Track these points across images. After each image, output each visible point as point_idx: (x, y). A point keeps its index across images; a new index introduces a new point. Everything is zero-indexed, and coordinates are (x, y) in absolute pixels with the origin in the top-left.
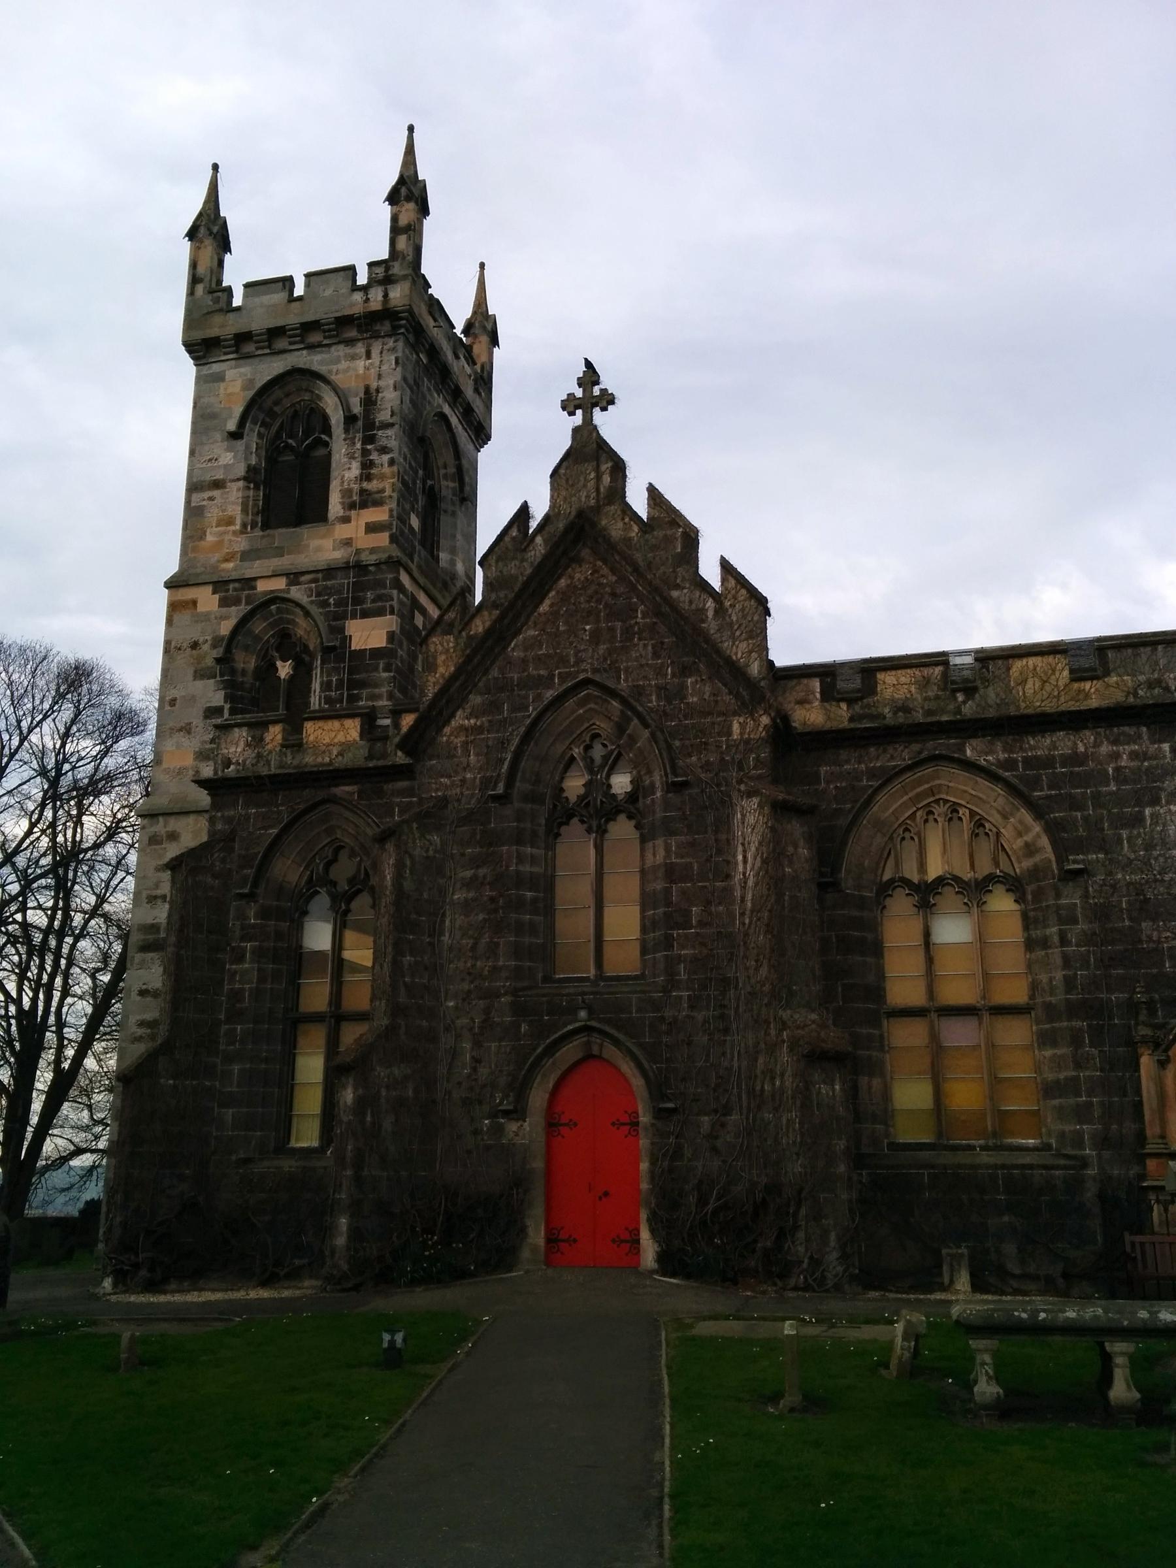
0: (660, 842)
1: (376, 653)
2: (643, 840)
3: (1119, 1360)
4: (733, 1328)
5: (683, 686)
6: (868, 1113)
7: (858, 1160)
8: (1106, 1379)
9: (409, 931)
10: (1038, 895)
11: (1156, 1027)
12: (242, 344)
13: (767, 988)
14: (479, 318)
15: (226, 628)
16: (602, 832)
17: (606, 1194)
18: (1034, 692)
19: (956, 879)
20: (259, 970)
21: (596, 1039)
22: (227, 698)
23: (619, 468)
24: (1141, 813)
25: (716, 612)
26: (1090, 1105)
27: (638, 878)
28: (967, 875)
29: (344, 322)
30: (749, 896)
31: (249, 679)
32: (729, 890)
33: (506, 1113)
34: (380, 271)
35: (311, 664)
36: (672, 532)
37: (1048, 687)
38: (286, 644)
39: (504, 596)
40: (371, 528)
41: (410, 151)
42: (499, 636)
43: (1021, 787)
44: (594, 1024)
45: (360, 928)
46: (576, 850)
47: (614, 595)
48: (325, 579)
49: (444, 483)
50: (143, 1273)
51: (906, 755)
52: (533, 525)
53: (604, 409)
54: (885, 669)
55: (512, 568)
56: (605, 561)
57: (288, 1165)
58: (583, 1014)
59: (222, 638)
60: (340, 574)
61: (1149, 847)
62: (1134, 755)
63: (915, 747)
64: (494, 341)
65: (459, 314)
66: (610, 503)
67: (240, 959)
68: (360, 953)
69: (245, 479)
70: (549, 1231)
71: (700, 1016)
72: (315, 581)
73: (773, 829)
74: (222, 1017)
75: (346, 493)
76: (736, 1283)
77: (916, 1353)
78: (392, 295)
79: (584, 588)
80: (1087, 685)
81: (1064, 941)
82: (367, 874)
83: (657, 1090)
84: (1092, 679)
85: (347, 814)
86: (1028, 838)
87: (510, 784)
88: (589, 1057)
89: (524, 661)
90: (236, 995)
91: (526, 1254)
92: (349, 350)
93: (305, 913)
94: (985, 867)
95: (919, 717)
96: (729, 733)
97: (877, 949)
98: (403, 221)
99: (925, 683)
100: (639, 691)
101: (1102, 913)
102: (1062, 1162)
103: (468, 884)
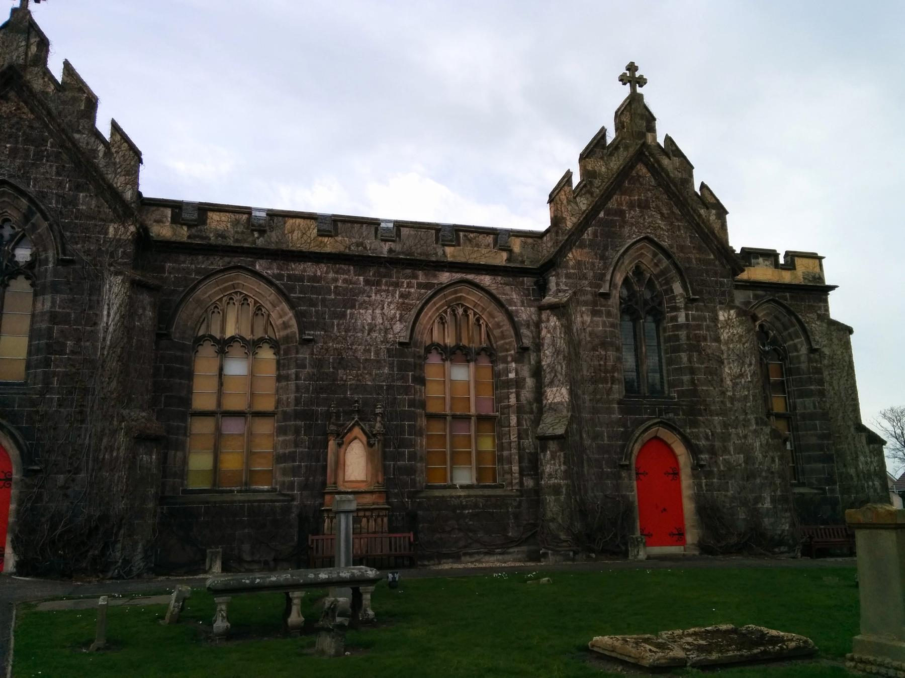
0: (48, 297)
2: (36, 295)
3: (295, 601)
5: (76, 198)
6: (172, 471)
8: (288, 612)
10: (287, 352)
13: (115, 395)
18: (299, 238)
19: (243, 339)
23: (44, 43)
24: (345, 312)
25: (105, 154)
26: (300, 466)
28: (248, 337)
30: (109, 338)
32: (94, 333)
37: (305, 237)
56: (26, 103)
61: (347, 330)
63: (227, 259)
73: (130, 297)
77: (182, 609)
79: (8, 118)
80: (326, 239)
81: (297, 378)
84: (329, 236)
86: (285, 319)
94: (259, 333)
95: (231, 242)
96: (106, 233)
97: (189, 375)
101: (319, 364)
102: (281, 498)
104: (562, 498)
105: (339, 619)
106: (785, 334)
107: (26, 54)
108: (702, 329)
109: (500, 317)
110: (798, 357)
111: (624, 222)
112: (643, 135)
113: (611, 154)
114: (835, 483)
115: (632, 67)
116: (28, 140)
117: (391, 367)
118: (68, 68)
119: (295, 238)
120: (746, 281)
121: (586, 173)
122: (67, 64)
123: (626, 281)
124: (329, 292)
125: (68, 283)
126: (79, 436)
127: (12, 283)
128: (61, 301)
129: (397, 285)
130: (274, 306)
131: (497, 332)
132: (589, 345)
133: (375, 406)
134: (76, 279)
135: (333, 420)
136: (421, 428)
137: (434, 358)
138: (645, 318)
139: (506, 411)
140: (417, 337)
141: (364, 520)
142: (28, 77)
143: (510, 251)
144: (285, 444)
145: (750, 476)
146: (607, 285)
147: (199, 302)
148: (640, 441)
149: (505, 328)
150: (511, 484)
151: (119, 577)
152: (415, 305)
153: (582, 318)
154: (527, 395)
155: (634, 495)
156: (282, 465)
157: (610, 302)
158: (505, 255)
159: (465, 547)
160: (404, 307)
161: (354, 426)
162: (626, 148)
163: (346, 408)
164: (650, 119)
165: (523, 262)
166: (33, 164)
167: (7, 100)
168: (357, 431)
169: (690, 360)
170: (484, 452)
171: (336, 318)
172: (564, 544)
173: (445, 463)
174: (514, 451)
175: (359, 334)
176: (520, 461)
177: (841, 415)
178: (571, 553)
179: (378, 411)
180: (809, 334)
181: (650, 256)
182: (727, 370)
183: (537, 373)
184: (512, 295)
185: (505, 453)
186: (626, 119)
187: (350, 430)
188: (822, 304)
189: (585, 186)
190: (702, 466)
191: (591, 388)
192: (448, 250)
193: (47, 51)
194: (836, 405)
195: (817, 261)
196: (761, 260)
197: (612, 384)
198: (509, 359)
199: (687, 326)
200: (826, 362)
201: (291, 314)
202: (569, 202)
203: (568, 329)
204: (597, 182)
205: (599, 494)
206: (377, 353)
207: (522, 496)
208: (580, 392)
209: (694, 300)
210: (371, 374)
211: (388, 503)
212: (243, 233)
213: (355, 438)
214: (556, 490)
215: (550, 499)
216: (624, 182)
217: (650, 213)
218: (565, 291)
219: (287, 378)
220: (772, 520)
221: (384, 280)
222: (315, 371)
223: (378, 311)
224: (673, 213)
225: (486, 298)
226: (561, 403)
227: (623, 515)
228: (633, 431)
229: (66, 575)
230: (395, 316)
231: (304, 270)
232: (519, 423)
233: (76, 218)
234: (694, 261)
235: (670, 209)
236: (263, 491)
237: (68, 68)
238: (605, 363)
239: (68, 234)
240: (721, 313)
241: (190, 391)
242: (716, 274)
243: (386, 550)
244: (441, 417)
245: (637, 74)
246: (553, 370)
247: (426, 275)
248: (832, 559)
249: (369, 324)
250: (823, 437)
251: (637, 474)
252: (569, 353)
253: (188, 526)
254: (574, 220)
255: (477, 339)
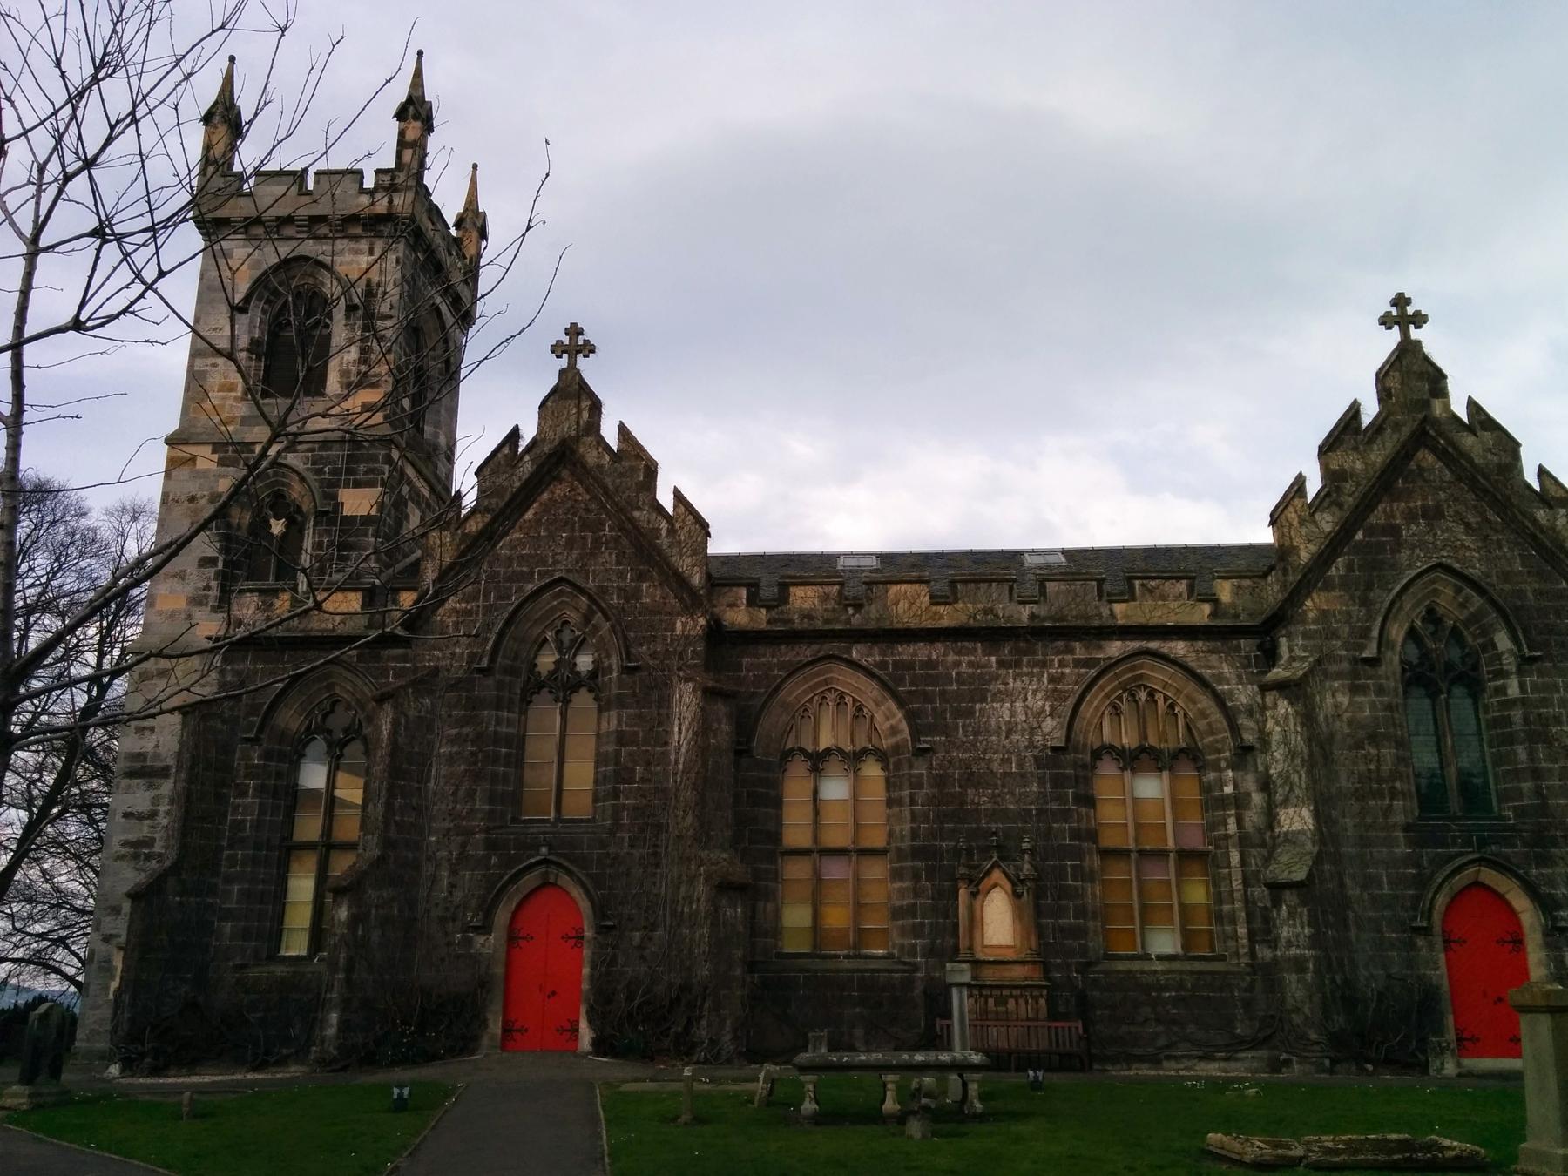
0: (613, 713)
1: (367, 520)
2: (600, 710)
3: (889, 1086)
4: (649, 1086)
5: (638, 589)
6: (762, 930)
7: (751, 967)
8: (883, 1101)
9: (401, 777)
10: (898, 766)
11: (970, 867)
12: (255, 227)
13: (691, 832)
14: (470, 215)
15: (224, 486)
16: (567, 702)
17: (554, 993)
18: (907, 604)
19: (840, 750)
20: (261, 804)
21: (553, 869)
22: (222, 550)
23: (596, 406)
24: (973, 708)
25: (668, 531)
26: (922, 925)
27: (594, 739)
28: (849, 748)
29: (353, 219)
30: (681, 760)
31: (243, 533)
32: (665, 754)
33: (476, 929)
34: (386, 179)
35: (303, 524)
36: (636, 464)
37: (914, 608)
38: (280, 503)
39: (497, 503)
40: (368, 408)
41: (418, 74)
42: (489, 536)
43: (890, 683)
44: (551, 857)
45: (352, 770)
46: (545, 717)
47: (587, 510)
48: (320, 449)
49: (432, 363)
50: (148, 1060)
51: (808, 653)
52: (523, 444)
53: (586, 356)
54: (796, 585)
55: (501, 479)
56: (581, 482)
57: (279, 970)
58: (544, 850)
59: (220, 495)
60: (336, 446)
61: (977, 733)
62: (970, 664)
63: (815, 647)
64: (483, 235)
65: (451, 206)
66: (587, 435)
67: (244, 794)
68: (351, 791)
69: (248, 350)
70: (505, 1022)
71: (637, 853)
72: (312, 450)
73: (702, 709)
74: (225, 844)
75: (344, 374)
76: (652, 1059)
77: (771, 1092)
78: (396, 202)
79: (563, 502)
80: (941, 609)
81: (913, 802)
82: (360, 724)
83: (600, 911)
84: (945, 604)
85: (346, 673)
86: (893, 722)
87: (492, 660)
88: (546, 884)
89: (510, 559)
90: (238, 826)
91: (485, 1041)
92: (352, 245)
93: (302, 756)
94: (862, 742)
95: (819, 625)
96: (674, 630)
97: (778, 803)
98: (411, 136)
99: (825, 598)
100: (603, 590)
101: (940, 781)
102: (901, 967)
103: (452, 741)
104: (1309, 977)
105: (924, 1101)
108: (1552, 705)
109: (1205, 702)
111: (1398, 545)
112: (1427, 405)
113: (1370, 441)
115: (1401, 301)
116: (585, 526)
117: (1042, 783)
119: (901, 611)
122: (622, 427)
123: (1412, 634)
125: (634, 694)
127: (575, 697)
129: (1044, 664)
131: (1202, 724)
132: (1349, 741)
134: (644, 690)
136: (1092, 871)
137: (1108, 768)
138: (1449, 691)
139: (1222, 843)
143: (1215, 601)
144: (902, 893)
146: (1374, 645)
149: (1213, 718)
150: (1237, 954)
152: (1073, 691)
153: (1334, 699)
154: (1255, 818)
155: (1439, 973)
158: (1207, 608)
159: (1167, 1047)
160: (1056, 696)
161: (992, 867)
162: (1397, 427)
164: (1436, 380)
165: (1237, 616)
167: (561, 480)
168: (997, 875)
169: (1532, 757)
170: (1195, 906)
171: (960, 717)
172: (1316, 1048)
173: (1132, 920)
174: (1238, 905)
178: (1327, 1062)
179: (1025, 846)
181: (1449, 592)
183: (1266, 785)
184: (1223, 668)
185: (1226, 908)
186: (1393, 383)
187: (988, 873)
189: (1328, 495)
191: (1356, 807)
192: (1118, 608)
197: (1392, 799)
198: (1223, 764)
199: (1523, 702)
201: (900, 715)
202: (1302, 522)
203: (1308, 718)
204: (1348, 486)
206: (1020, 764)
209: (1535, 659)
210: (1013, 794)
211: (1048, 979)
213: (995, 885)
214: (1299, 965)
215: (1291, 978)
218: (1303, 659)
221: (1025, 659)
223: (1019, 704)
224: (1488, 521)
225: (1180, 674)
226: (1302, 832)
227: (1422, 1009)
228: (1433, 873)
229: (647, 1056)
231: (915, 654)
232: (1243, 862)
234: (1530, 595)
238: (1378, 768)
243: (1044, 1045)
244: (1123, 854)
245: (1410, 310)
247: (1087, 648)
252: (1311, 755)
253: (784, 1001)
254: (1313, 548)
255: (1171, 737)
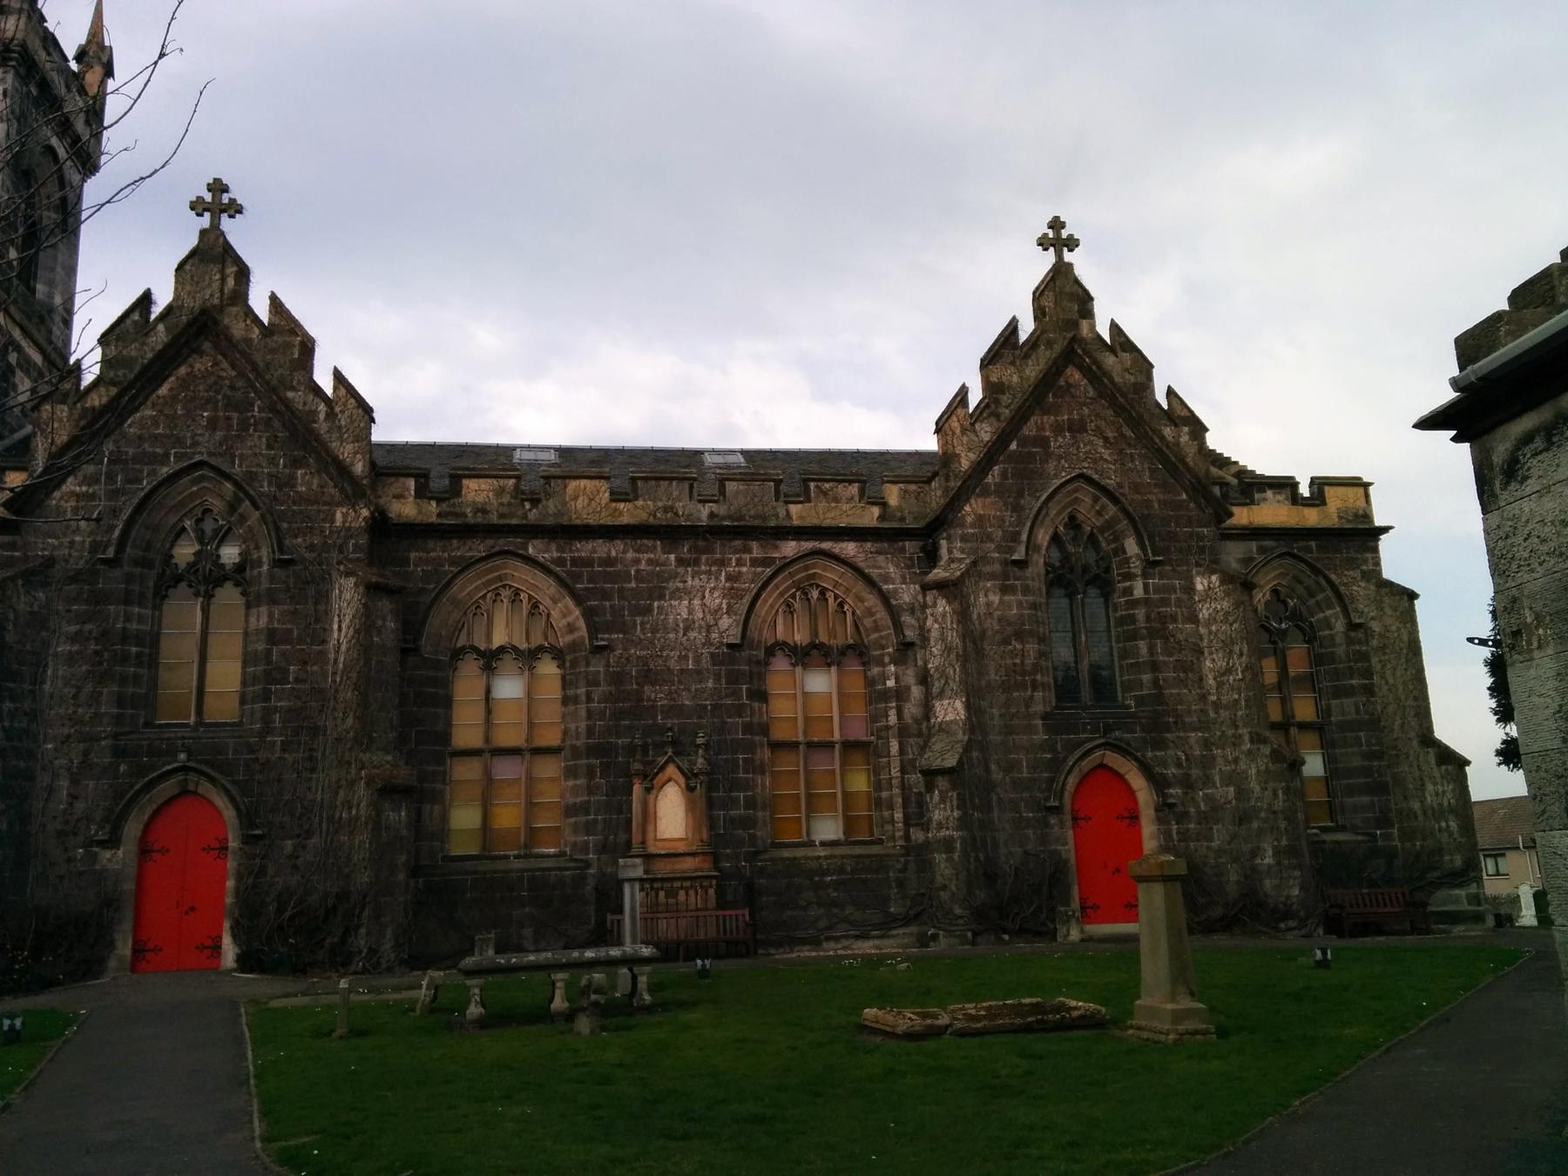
0: (264, 609)
2: (248, 606)
5: (293, 477)
6: (428, 830)
10: (574, 664)
18: (587, 500)
19: (514, 648)
23: (243, 274)
24: (651, 605)
25: (327, 415)
26: (595, 821)
28: (524, 646)
32: (323, 654)
56: (225, 356)
61: (654, 631)
63: (490, 542)
73: (365, 605)
80: (621, 505)
81: (589, 699)
84: (625, 501)
86: (570, 619)
94: (538, 640)
95: (494, 518)
96: (333, 521)
97: (447, 702)
101: (618, 678)
104: (956, 856)
105: (593, 997)
106: (1312, 602)
107: (222, 291)
109: (872, 600)
110: (1332, 637)
111: (1048, 455)
112: (1075, 325)
113: (1026, 356)
114: (1392, 826)
115: (1056, 224)
116: (230, 405)
117: (718, 679)
118: (276, 303)
120: (1244, 528)
121: (991, 388)
122: (274, 299)
123: (1056, 539)
124: (628, 578)
125: (288, 589)
126: (309, 789)
128: (281, 614)
129: (722, 563)
130: (555, 602)
131: (868, 622)
132: (998, 637)
133: (696, 735)
135: (638, 757)
137: (780, 663)
138: (1085, 592)
139: (883, 734)
140: (753, 633)
141: (682, 893)
142: (226, 321)
143: (884, 505)
144: (575, 791)
145: (1243, 818)
146: (1022, 549)
147: (456, 603)
148: (1076, 769)
149: (878, 616)
150: (893, 838)
151: (364, 971)
153: (987, 598)
154: (913, 710)
155: (1068, 850)
156: (572, 820)
157: (1029, 571)
158: (876, 511)
159: (829, 928)
160: (732, 594)
161: (666, 763)
162: (1049, 344)
163: (658, 738)
164: (1084, 301)
165: (903, 519)
166: (238, 436)
167: (201, 353)
168: (671, 770)
174: (896, 791)
175: (672, 636)
176: (905, 805)
177: (1398, 722)
178: (969, 934)
179: (700, 741)
180: (1347, 602)
181: (1088, 500)
182: (1208, 663)
183: (924, 679)
184: (888, 568)
185: (885, 794)
186: (1048, 302)
187: (662, 768)
188: (1369, 555)
189: (987, 406)
190: (1171, 806)
192: (794, 509)
193: (248, 281)
194: (1391, 708)
195: (1361, 490)
196: (1269, 494)
198: (887, 659)
199: (1146, 602)
200: (1375, 643)
202: (964, 431)
203: (963, 615)
205: (1017, 850)
206: (697, 660)
207: (907, 854)
208: (984, 704)
209: (1155, 564)
211: (717, 869)
212: (509, 504)
213: (669, 780)
214: (948, 845)
215: (940, 857)
216: (1046, 396)
217: (1087, 438)
218: (960, 560)
219: (575, 700)
220: (1276, 882)
221: (704, 558)
222: (613, 688)
223: (696, 602)
224: (1124, 436)
225: (850, 574)
227: (1056, 878)
228: (1066, 758)
229: (299, 969)
230: (720, 608)
231: (594, 551)
232: (902, 751)
233: (294, 503)
235: (1118, 430)
236: (549, 856)
237: (276, 303)
239: (285, 525)
240: (1198, 579)
241: (449, 723)
242: (1190, 522)
243: (712, 933)
244: (793, 746)
245: (1064, 234)
246: (943, 674)
248: (1382, 938)
249: (685, 620)
250: (1371, 756)
251: (1075, 819)
252: (965, 650)
253: (448, 904)
255: (839, 629)
